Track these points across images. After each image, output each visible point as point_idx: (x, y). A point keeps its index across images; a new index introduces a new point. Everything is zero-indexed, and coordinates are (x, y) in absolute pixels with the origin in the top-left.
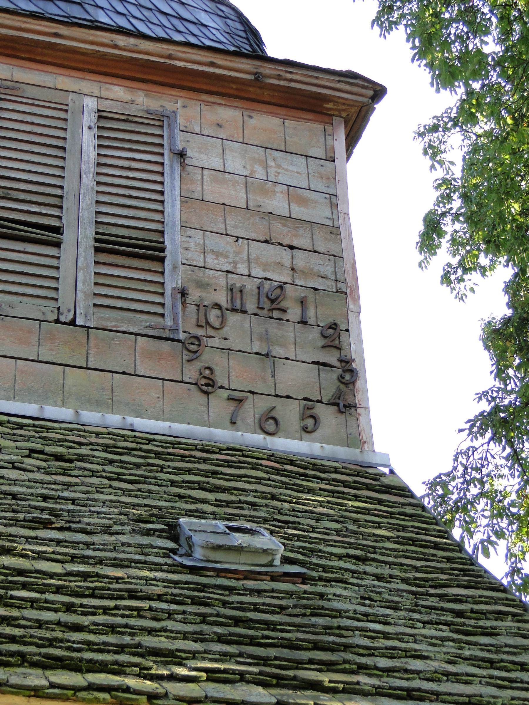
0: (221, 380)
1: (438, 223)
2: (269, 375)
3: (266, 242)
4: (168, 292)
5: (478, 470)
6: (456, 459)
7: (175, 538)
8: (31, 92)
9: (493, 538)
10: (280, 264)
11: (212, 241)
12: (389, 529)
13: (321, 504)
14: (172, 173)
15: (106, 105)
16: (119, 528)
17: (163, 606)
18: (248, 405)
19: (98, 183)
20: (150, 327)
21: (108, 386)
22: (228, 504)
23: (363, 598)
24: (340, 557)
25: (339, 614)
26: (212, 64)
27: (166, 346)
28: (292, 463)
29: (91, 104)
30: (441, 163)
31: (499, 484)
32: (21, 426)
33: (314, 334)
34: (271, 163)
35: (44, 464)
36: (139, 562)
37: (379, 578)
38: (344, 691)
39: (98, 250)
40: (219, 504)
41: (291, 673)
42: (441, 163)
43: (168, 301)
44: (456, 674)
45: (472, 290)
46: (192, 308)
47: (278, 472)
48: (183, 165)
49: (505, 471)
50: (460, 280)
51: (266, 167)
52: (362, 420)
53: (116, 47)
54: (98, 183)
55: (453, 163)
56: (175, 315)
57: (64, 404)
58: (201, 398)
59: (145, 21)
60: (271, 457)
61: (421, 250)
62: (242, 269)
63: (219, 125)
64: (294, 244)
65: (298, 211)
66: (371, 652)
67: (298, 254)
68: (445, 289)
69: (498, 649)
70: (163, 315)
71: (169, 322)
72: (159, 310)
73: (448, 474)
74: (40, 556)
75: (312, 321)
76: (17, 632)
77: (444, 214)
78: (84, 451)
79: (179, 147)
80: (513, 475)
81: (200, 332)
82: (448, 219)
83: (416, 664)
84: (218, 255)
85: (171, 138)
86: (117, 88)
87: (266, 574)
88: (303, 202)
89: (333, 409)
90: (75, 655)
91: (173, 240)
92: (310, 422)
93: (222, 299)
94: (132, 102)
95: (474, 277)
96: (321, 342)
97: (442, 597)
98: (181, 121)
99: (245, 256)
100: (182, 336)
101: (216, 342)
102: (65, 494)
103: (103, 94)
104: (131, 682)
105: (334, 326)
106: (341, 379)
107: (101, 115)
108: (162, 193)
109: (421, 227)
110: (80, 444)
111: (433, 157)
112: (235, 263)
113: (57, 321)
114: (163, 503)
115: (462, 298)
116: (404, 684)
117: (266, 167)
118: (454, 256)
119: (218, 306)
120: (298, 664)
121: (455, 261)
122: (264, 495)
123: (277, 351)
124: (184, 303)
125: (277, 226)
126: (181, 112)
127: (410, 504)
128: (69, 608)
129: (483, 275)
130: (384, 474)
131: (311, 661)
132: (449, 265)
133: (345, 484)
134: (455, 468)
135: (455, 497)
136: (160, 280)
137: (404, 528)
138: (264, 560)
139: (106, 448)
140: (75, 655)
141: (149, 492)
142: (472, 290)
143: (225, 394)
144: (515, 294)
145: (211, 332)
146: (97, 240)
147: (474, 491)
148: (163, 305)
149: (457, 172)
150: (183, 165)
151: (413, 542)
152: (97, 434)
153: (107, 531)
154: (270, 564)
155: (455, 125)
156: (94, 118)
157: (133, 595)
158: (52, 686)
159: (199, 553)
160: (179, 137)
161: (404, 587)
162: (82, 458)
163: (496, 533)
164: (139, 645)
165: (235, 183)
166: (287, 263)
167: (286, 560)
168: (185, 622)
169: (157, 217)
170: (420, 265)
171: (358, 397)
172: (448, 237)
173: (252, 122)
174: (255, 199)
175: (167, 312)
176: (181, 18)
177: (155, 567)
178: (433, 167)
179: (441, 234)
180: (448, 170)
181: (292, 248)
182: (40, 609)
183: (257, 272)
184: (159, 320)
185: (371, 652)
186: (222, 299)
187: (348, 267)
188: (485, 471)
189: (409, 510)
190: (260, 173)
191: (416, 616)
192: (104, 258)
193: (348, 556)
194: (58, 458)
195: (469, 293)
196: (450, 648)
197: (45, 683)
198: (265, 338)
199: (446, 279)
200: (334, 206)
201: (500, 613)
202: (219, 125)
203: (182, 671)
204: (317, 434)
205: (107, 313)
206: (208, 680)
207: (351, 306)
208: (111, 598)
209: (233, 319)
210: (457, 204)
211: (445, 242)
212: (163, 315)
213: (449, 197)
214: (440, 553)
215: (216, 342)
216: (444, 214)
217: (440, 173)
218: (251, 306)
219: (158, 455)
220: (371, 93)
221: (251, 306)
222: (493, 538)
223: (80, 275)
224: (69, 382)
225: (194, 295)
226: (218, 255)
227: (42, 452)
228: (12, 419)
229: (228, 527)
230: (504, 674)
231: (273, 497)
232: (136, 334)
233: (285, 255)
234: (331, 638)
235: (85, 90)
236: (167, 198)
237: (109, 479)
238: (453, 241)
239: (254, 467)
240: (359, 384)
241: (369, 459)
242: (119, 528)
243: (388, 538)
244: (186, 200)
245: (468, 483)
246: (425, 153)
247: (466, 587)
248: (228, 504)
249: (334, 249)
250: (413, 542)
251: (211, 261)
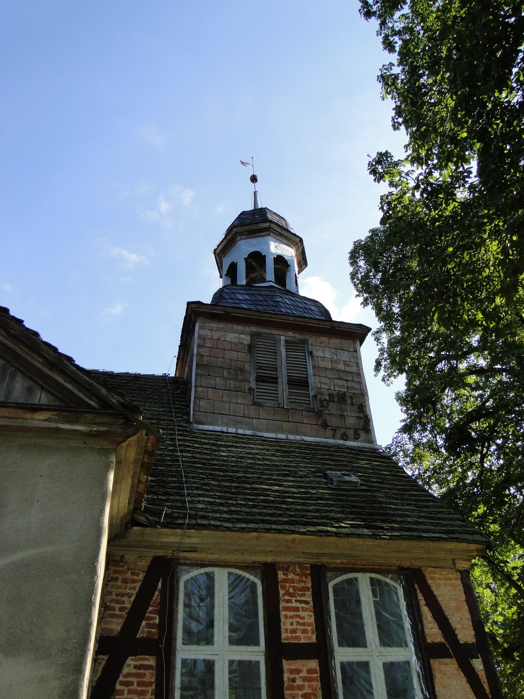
0: (329, 424)
1: (380, 362)
2: (343, 421)
3: (339, 379)
4: (311, 396)
5: (399, 443)
6: (393, 440)
7: (326, 478)
8: (265, 335)
9: (405, 465)
10: (344, 386)
11: (323, 380)
12: (387, 472)
13: (366, 464)
14: (309, 359)
15: (288, 338)
16: (310, 475)
17: (330, 502)
18: (338, 432)
19: (287, 363)
20: (306, 408)
21: (295, 427)
22: (339, 465)
23: (387, 497)
24: (375, 482)
25: (382, 502)
26: (319, 324)
27: (311, 414)
28: (354, 450)
29: (283, 338)
30: (380, 343)
31: (407, 447)
32: (272, 442)
33: (356, 408)
34: (338, 354)
35: (282, 454)
36: (318, 487)
37: (389, 489)
38: (390, 529)
39: (289, 384)
40: (335, 465)
41: (373, 524)
42: (380, 343)
43: (311, 399)
44: (421, 522)
45: (392, 383)
46: (318, 401)
47: (350, 453)
48: (312, 356)
49: (408, 443)
50: (388, 380)
51: (337, 355)
52: (372, 434)
53: (290, 320)
54: (287, 363)
55: (384, 343)
56: (314, 405)
57: (283, 433)
58: (323, 430)
59: (296, 310)
60: (347, 448)
61: (375, 371)
62: (332, 388)
63: (322, 343)
64: (347, 379)
65: (347, 369)
66: (394, 515)
67: (349, 382)
68: (383, 383)
69: (431, 513)
70: (310, 404)
71: (312, 406)
72: (309, 402)
73: (390, 445)
74: (290, 486)
75: (355, 403)
76: (292, 513)
77: (382, 359)
78: (292, 449)
79: (310, 350)
80: (411, 444)
81: (321, 409)
82: (383, 361)
83: (409, 519)
84: (325, 384)
85: (308, 348)
86: (290, 333)
87: (356, 489)
88: (349, 366)
89: (363, 432)
90: (310, 520)
91: (311, 379)
92: (357, 436)
93: (327, 397)
94: (295, 337)
95: (392, 379)
96: (358, 410)
97: (409, 495)
98: (310, 342)
99: (332, 384)
100: (316, 410)
101: (326, 412)
102: (291, 464)
103: (287, 335)
104: (329, 529)
105: (362, 405)
106: (365, 421)
107: (286, 342)
108: (306, 365)
109: (375, 364)
110: (291, 447)
111: (377, 342)
112: (330, 386)
113: (279, 407)
114: (319, 466)
115: (388, 385)
116: (407, 526)
117: (337, 355)
118: (385, 372)
119: (326, 400)
120: (375, 521)
121: (386, 374)
122: (348, 462)
123: (345, 414)
124: (316, 400)
125: (342, 374)
126: (310, 339)
127: (391, 462)
128: (304, 504)
129: (395, 378)
130: (381, 452)
131: (378, 520)
132: (384, 375)
133: (371, 456)
134: (393, 443)
135: (393, 452)
136: (307, 393)
137: (392, 471)
138: (355, 485)
139: (298, 448)
140: (310, 520)
141: (315, 462)
142: (392, 383)
143: (330, 428)
144: (409, 386)
145: (325, 409)
146: (288, 381)
147: (399, 449)
148: (309, 401)
149: (386, 345)
150: (312, 356)
151: (395, 476)
152: (295, 443)
153: (306, 476)
154: (357, 486)
155: (384, 331)
156: (284, 342)
157: (320, 499)
158: (308, 531)
159: (335, 484)
160: (310, 347)
161: (398, 492)
162: (293, 452)
163: (406, 463)
164: (328, 516)
165: (328, 361)
166: (345, 385)
167: (361, 484)
168: (337, 507)
169: (305, 373)
170: (375, 376)
171: (371, 427)
172: (383, 366)
173: (331, 341)
174: (334, 366)
175: (311, 403)
176: (306, 308)
177: (324, 489)
178: (377, 344)
179: (381, 365)
180: (382, 345)
181: (346, 380)
182: (296, 505)
183: (337, 389)
184: (309, 405)
185: (394, 515)
186: (327, 397)
187: (364, 386)
188: (402, 443)
189: (392, 465)
190: (335, 357)
191: (404, 502)
192: (291, 387)
193: (378, 482)
194: (286, 452)
195: (391, 384)
196: (416, 513)
197: (305, 530)
198: (341, 410)
199: (383, 380)
200: (358, 366)
201: (428, 500)
202: (322, 343)
203: (343, 525)
204: (359, 440)
205: (293, 404)
206: (351, 527)
207: (366, 398)
208: (314, 500)
209: (331, 404)
210: (386, 355)
211: (382, 369)
212: (310, 404)
213: (383, 353)
214: (404, 479)
215: (326, 412)
216: (382, 359)
217: (380, 346)
218: (336, 400)
219: (314, 449)
220: (367, 330)
221: (336, 400)
222: (405, 465)
223: (284, 393)
224: (284, 426)
225: (319, 397)
226: (325, 384)
227: (280, 450)
228: (269, 439)
229: (342, 474)
230: (435, 521)
231: (351, 462)
232: (302, 410)
233: (345, 383)
234: (382, 511)
235: (281, 334)
236: (308, 367)
237: (302, 458)
238: (385, 367)
239: (343, 452)
240: (371, 423)
241: (376, 447)
242: (310, 475)
243: (388, 475)
244: (314, 367)
245: (397, 447)
246: (375, 340)
247: (416, 491)
248: (339, 465)
249: (359, 380)
250: (395, 476)
251: (323, 386)
